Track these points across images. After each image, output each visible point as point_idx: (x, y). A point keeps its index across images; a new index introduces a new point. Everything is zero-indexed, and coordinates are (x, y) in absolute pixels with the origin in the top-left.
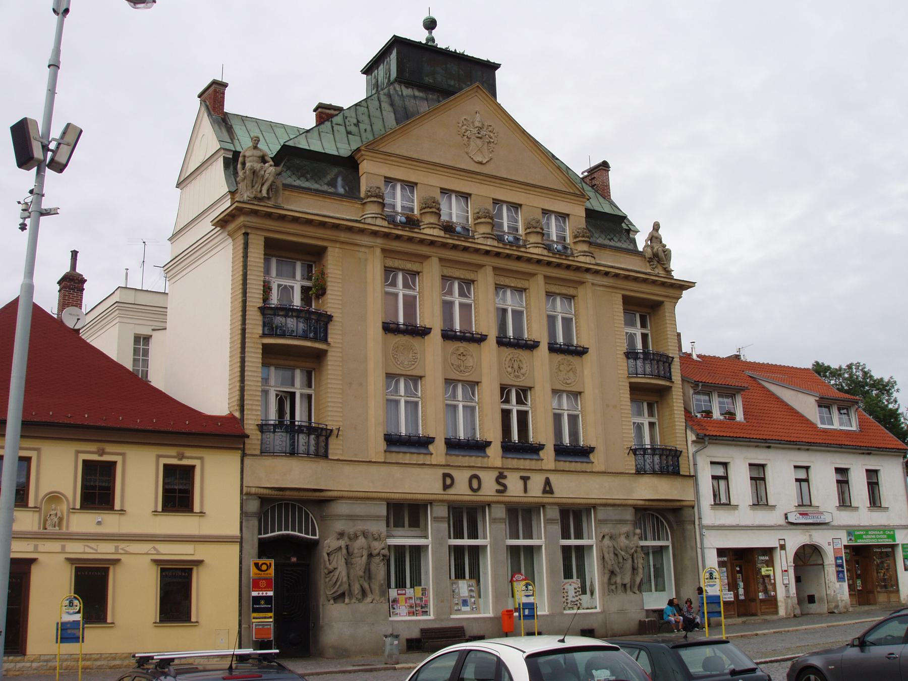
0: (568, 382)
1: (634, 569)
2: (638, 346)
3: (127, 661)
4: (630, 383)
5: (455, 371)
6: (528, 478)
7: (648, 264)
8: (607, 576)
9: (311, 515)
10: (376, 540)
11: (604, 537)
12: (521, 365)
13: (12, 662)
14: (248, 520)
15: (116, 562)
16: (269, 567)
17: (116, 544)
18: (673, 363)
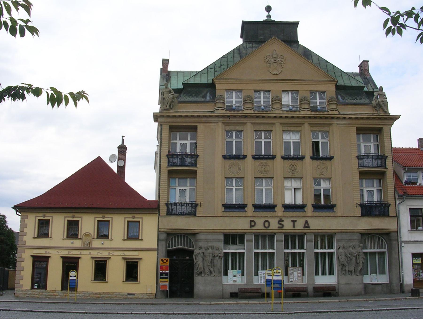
0: (322, 173)
1: (357, 264)
2: (372, 151)
3: (113, 296)
4: (359, 171)
5: (260, 174)
6: (296, 221)
7: (374, 109)
8: (341, 267)
9: (191, 240)
10: (217, 250)
11: (339, 248)
12: (296, 168)
13: (73, 293)
14: (161, 242)
15: (109, 258)
16: (167, 261)
17: (109, 252)
18: (387, 159)
